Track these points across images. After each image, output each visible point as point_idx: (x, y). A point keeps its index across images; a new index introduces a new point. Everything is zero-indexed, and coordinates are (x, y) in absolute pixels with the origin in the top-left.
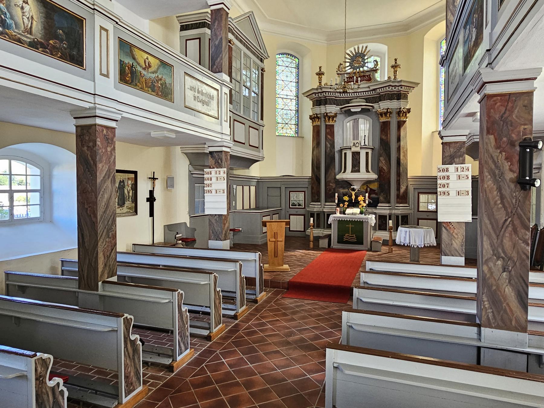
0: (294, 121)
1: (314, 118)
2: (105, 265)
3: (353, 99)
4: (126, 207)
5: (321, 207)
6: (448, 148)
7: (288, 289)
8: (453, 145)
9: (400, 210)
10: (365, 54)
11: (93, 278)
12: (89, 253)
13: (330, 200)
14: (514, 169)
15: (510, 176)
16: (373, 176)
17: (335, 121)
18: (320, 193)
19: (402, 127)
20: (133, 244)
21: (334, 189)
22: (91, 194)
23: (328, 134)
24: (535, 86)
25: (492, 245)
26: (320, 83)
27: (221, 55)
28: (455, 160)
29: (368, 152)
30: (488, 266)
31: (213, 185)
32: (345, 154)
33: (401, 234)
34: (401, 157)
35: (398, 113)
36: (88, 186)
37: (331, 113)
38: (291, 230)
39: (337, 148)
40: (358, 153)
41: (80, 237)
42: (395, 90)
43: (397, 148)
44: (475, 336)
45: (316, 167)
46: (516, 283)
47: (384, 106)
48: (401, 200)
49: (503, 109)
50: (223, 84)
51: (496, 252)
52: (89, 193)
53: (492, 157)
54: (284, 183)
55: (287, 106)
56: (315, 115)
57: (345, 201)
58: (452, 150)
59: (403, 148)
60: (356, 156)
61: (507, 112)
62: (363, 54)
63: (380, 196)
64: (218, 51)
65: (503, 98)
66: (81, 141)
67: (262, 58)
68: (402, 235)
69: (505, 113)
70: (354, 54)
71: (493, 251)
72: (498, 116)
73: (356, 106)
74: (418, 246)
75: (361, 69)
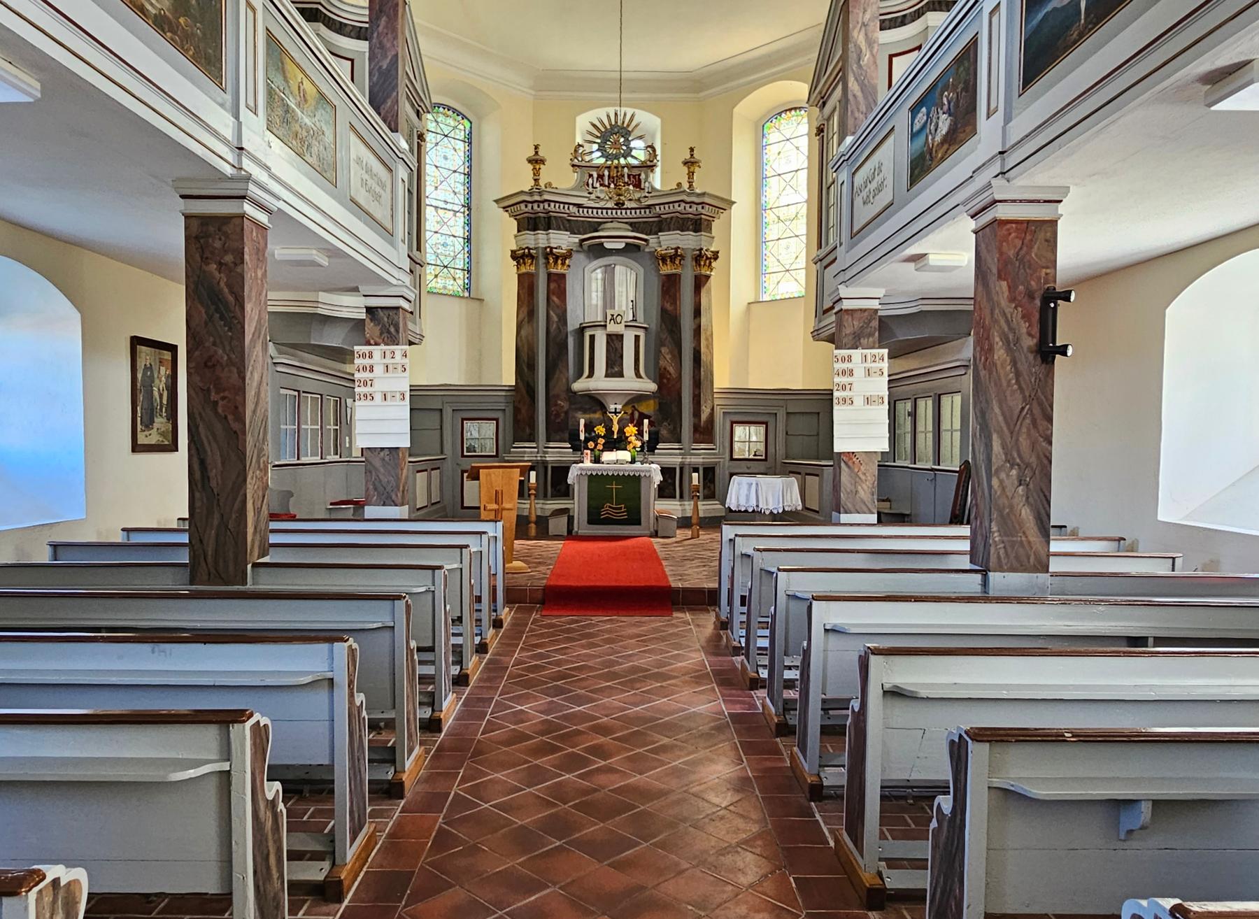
0: (462, 263)
1: (523, 256)
2: (255, 528)
3: (607, 222)
4: (155, 430)
5: (538, 452)
6: (850, 319)
7: (543, 603)
8: (857, 315)
9: (700, 455)
10: (630, 129)
12: (222, 501)
13: (558, 437)
14: (1033, 333)
15: (1029, 342)
16: (650, 386)
17: (569, 266)
18: (534, 421)
19: (704, 286)
20: (179, 519)
21: (566, 413)
22: (226, 369)
23: (554, 294)
24: (1060, 212)
25: (1004, 446)
26: (535, 180)
27: (395, 94)
28: (862, 340)
29: (639, 336)
30: (998, 478)
31: (375, 382)
32: (592, 338)
33: (739, 489)
35: (696, 258)
36: (220, 352)
37: (559, 247)
39: (573, 324)
40: (620, 337)
41: (196, 466)
44: (979, 588)
45: (525, 363)
46: (1035, 500)
47: (671, 242)
49: (1018, 243)
50: (403, 159)
51: (1009, 457)
52: (222, 366)
53: (1004, 314)
54: (450, 399)
56: (526, 251)
57: (599, 436)
59: (706, 330)
60: (615, 342)
61: (1025, 249)
63: (662, 429)
65: (1019, 226)
66: (200, 250)
67: (420, 109)
68: (741, 491)
69: (1021, 248)
70: (609, 127)
71: (1006, 454)
72: (1012, 252)
73: (615, 235)
74: (771, 512)
75: (622, 161)
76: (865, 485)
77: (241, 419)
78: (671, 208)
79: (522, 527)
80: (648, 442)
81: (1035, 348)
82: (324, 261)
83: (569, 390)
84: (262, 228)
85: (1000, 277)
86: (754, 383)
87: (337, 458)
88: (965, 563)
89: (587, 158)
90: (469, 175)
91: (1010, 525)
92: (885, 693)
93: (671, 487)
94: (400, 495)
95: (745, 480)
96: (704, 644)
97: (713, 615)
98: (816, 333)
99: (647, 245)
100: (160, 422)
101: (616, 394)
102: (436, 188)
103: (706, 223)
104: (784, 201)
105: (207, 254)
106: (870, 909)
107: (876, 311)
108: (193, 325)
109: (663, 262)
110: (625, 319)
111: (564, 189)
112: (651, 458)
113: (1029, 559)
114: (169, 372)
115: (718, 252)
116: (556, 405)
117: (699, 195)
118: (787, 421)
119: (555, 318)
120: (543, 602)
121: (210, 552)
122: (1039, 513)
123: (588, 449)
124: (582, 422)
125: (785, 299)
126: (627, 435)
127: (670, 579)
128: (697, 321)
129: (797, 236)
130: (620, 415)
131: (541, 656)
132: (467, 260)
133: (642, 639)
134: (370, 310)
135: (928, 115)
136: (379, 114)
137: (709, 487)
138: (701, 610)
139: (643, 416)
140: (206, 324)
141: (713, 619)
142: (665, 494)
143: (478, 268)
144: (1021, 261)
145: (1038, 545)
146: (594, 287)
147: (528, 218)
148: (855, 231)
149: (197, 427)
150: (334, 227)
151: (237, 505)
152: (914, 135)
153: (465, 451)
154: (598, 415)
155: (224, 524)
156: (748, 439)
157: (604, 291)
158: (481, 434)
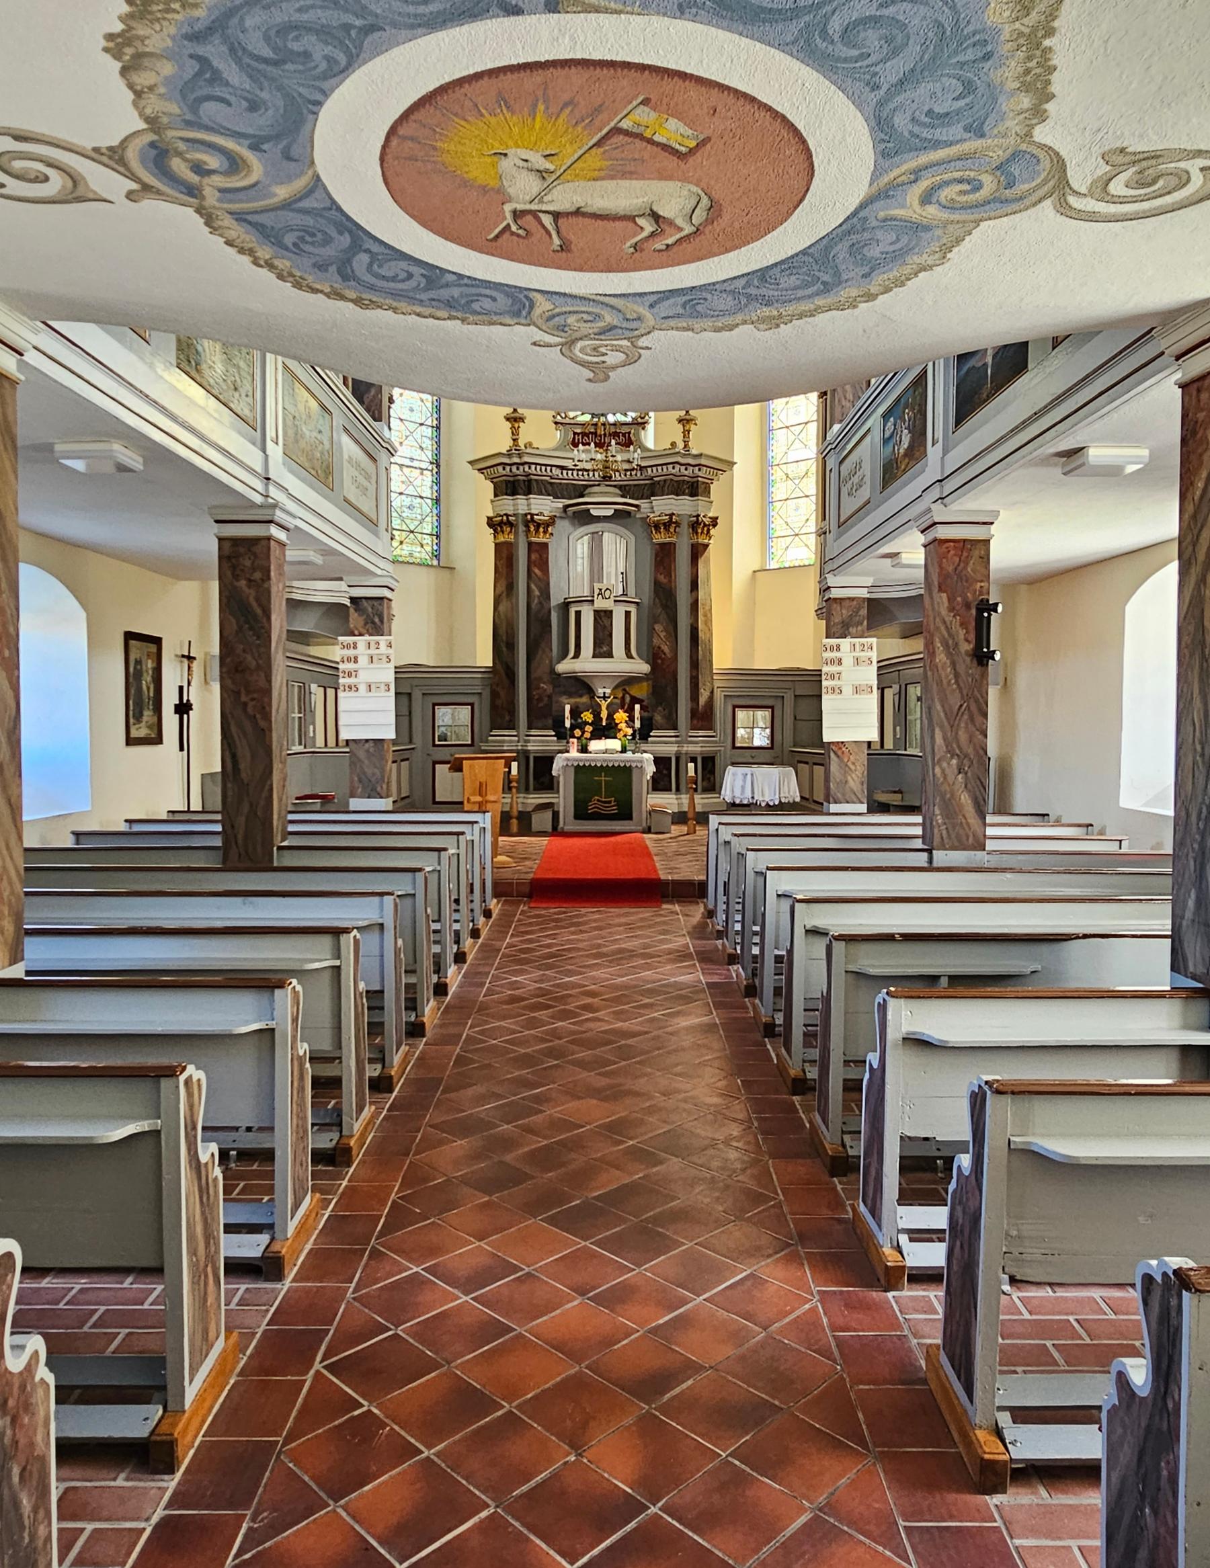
0: (430, 526)
1: (501, 523)
5: (518, 742)
6: (839, 608)
8: (847, 603)
9: (699, 743)
13: (540, 725)
14: (970, 639)
15: (966, 647)
17: (552, 534)
19: (702, 555)
20: (169, 812)
21: (550, 697)
25: (945, 739)
26: (514, 440)
28: (851, 629)
29: (630, 612)
30: (941, 768)
31: (361, 674)
32: (578, 614)
34: (701, 626)
36: (249, 658)
37: (541, 514)
38: (437, 800)
39: (556, 599)
40: (609, 614)
41: (229, 761)
42: (686, 473)
45: (503, 641)
48: (700, 723)
53: (944, 622)
55: (411, 487)
56: (505, 518)
57: (586, 723)
58: (844, 612)
60: (603, 619)
61: (962, 565)
65: (956, 545)
68: (736, 782)
69: (959, 565)
71: (947, 747)
76: (856, 775)
77: (267, 716)
78: (665, 470)
79: (504, 825)
80: (639, 729)
81: (971, 653)
83: (553, 671)
84: (282, 545)
85: (940, 590)
87: (301, 749)
88: (918, 844)
90: (438, 428)
92: (807, 931)
93: (666, 779)
94: (385, 786)
95: (741, 770)
96: (691, 930)
98: (819, 612)
99: (639, 510)
100: (148, 715)
101: (604, 677)
103: (703, 486)
104: (792, 456)
105: (238, 572)
106: (794, 1094)
108: (225, 634)
109: (656, 530)
111: (549, 450)
112: (644, 747)
113: (968, 839)
114: (155, 665)
115: (717, 518)
116: (538, 688)
118: (795, 706)
120: (530, 896)
121: (240, 837)
123: (574, 737)
124: (568, 708)
125: (795, 567)
127: (660, 872)
129: (807, 496)
130: (609, 700)
131: (530, 941)
132: (436, 524)
133: (630, 927)
134: (354, 600)
136: (361, 402)
137: (709, 779)
138: (690, 902)
141: (702, 909)
143: (448, 531)
144: (960, 577)
149: (229, 724)
152: (885, 441)
153: (437, 741)
154: (585, 699)
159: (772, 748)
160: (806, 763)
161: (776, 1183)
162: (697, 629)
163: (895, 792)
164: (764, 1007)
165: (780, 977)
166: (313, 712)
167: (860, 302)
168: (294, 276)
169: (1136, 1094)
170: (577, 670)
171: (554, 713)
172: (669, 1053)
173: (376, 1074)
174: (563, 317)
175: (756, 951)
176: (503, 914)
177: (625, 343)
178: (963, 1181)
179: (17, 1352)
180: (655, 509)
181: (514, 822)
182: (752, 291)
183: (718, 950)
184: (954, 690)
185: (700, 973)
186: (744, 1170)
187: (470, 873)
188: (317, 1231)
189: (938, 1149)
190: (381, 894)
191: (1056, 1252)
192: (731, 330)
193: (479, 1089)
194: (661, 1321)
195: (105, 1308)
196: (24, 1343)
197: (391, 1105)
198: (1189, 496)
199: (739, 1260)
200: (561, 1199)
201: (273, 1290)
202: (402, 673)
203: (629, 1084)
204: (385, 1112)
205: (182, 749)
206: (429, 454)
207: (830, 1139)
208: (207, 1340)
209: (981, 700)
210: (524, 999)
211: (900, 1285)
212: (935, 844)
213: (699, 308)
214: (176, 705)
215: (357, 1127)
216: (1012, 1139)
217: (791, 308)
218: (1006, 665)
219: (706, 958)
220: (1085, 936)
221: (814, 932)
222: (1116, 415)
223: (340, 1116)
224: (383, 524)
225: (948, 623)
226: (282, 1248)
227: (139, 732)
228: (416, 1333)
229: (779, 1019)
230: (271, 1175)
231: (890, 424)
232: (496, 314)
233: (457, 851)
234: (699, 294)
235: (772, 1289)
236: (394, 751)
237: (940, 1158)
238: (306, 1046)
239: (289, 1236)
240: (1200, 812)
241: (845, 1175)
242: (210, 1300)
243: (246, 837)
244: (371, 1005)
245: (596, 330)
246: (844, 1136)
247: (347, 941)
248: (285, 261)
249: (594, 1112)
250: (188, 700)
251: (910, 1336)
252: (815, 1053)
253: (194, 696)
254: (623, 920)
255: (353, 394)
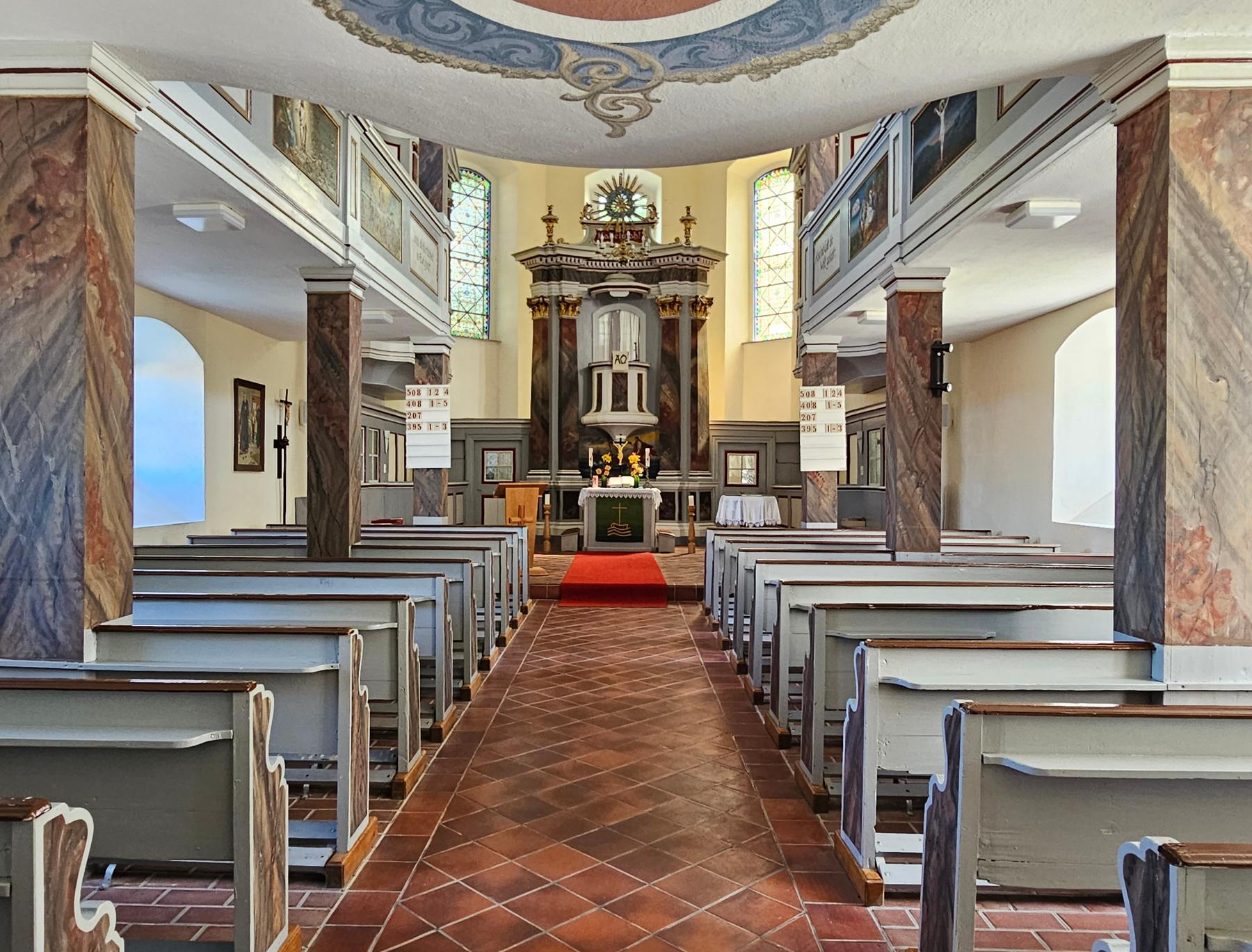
1: (538, 304)
6: (813, 361)
9: (697, 481)
10: (633, 190)
11: (338, 540)
12: (331, 500)
13: (569, 465)
15: (923, 381)
17: (579, 312)
21: (577, 443)
22: (335, 404)
25: (905, 458)
27: (440, 181)
28: (823, 379)
30: (902, 482)
32: (600, 376)
36: (331, 391)
39: (582, 364)
40: (625, 375)
41: (313, 475)
42: (687, 262)
43: (692, 369)
45: (539, 399)
49: (914, 309)
52: (332, 401)
56: (541, 299)
58: (818, 364)
60: (620, 379)
61: (919, 313)
62: (629, 190)
64: (434, 173)
65: (915, 297)
69: (916, 313)
70: (614, 189)
71: (907, 464)
73: (620, 286)
76: (828, 502)
77: (345, 439)
79: (539, 544)
80: (649, 468)
81: (927, 386)
82: (390, 319)
83: (579, 422)
86: (749, 416)
87: (376, 482)
88: (884, 548)
89: (595, 216)
90: (488, 230)
91: (911, 517)
92: (791, 610)
94: (442, 508)
95: (732, 498)
97: (700, 606)
99: (649, 293)
100: (252, 447)
101: (621, 427)
102: (459, 242)
106: (781, 749)
107: (835, 354)
109: (663, 308)
110: (629, 359)
114: (259, 407)
117: (695, 249)
119: (566, 359)
122: (932, 508)
123: (596, 474)
124: (591, 451)
126: (631, 462)
127: (665, 575)
128: (694, 360)
129: (785, 283)
131: (560, 631)
132: (486, 306)
133: (641, 622)
134: (419, 356)
135: (861, 205)
136: (428, 197)
139: (645, 446)
140: (321, 370)
142: (666, 516)
145: (932, 531)
146: (601, 331)
147: (543, 270)
148: (816, 289)
150: (383, 280)
151: (342, 501)
152: (853, 219)
153: (484, 478)
154: (605, 446)
155: (332, 517)
156: (742, 468)
157: (611, 334)
158: (499, 462)
159: (757, 485)
160: (786, 497)
161: (767, 818)
162: (696, 388)
163: (860, 520)
164: (754, 681)
165: (768, 657)
166: (387, 454)
167: (839, 49)
168: (362, 29)
169: (1099, 715)
170: (599, 421)
171: (580, 456)
172: (676, 715)
173: (428, 726)
174: (586, 68)
175: (746, 638)
176: (537, 611)
177: (639, 96)
178: (939, 797)
179: (87, 914)
180: (662, 291)
181: (548, 543)
182: (748, 38)
183: (715, 638)
184: (913, 417)
185: (700, 656)
186: (739, 807)
187: (510, 573)
188: (374, 849)
189: (907, 791)
190: (434, 576)
191: (1026, 860)
192: (728, 80)
193: (515, 741)
194: (668, 927)
195: (190, 906)
196: (95, 907)
197: (440, 752)
198: (1125, 217)
199: (736, 879)
200: (584, 827)
201: (334, 895)
202: (457, 426)
203: (641, 739)
204: (435, 757)
205: (279, 476)
206: (482, 250)
207: (812, 780)
208: (272, 929)
209: (936, 426)
210: (554, 674)
211: (878, 901)
212: (897, 546)
213: (702, 57)
214: (275, 441)
215: (411, 765)
216: (985, 755)
217: (779, 57)
218: (952, 410)
219: (704, 645)
220: (1034, 607)
221: (797, 610)
222: (1054, 168)
223: (396, 756)
224: (443, 294)
225: (907, 362)
226: (343, 859)
227: (245, 460)
228: (455, 932)
229: (767, 689)
230: (334, 804)
231: (857, 205)
232: (530, 66)
233: (499, 554)
234: (700, 43)
235: (766, 903)
236: (449, 486)
237: (909, 798)
238: (365, 688)
239: (348, 850)
240: (1139, 489)
241: (827, 812)
242: (276, 894)
243: (326, 538)
244: (424, 674)
245: (614, 82)
246: (825, 779)
247: (403, 607)
248: (353, 13)
249: (610, 761)
250: (285, 437)
251: (889, 944)
252: (799, 714)
253: (290, 434)
254: (635, 616)
255: (420, 187)
